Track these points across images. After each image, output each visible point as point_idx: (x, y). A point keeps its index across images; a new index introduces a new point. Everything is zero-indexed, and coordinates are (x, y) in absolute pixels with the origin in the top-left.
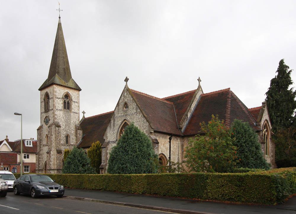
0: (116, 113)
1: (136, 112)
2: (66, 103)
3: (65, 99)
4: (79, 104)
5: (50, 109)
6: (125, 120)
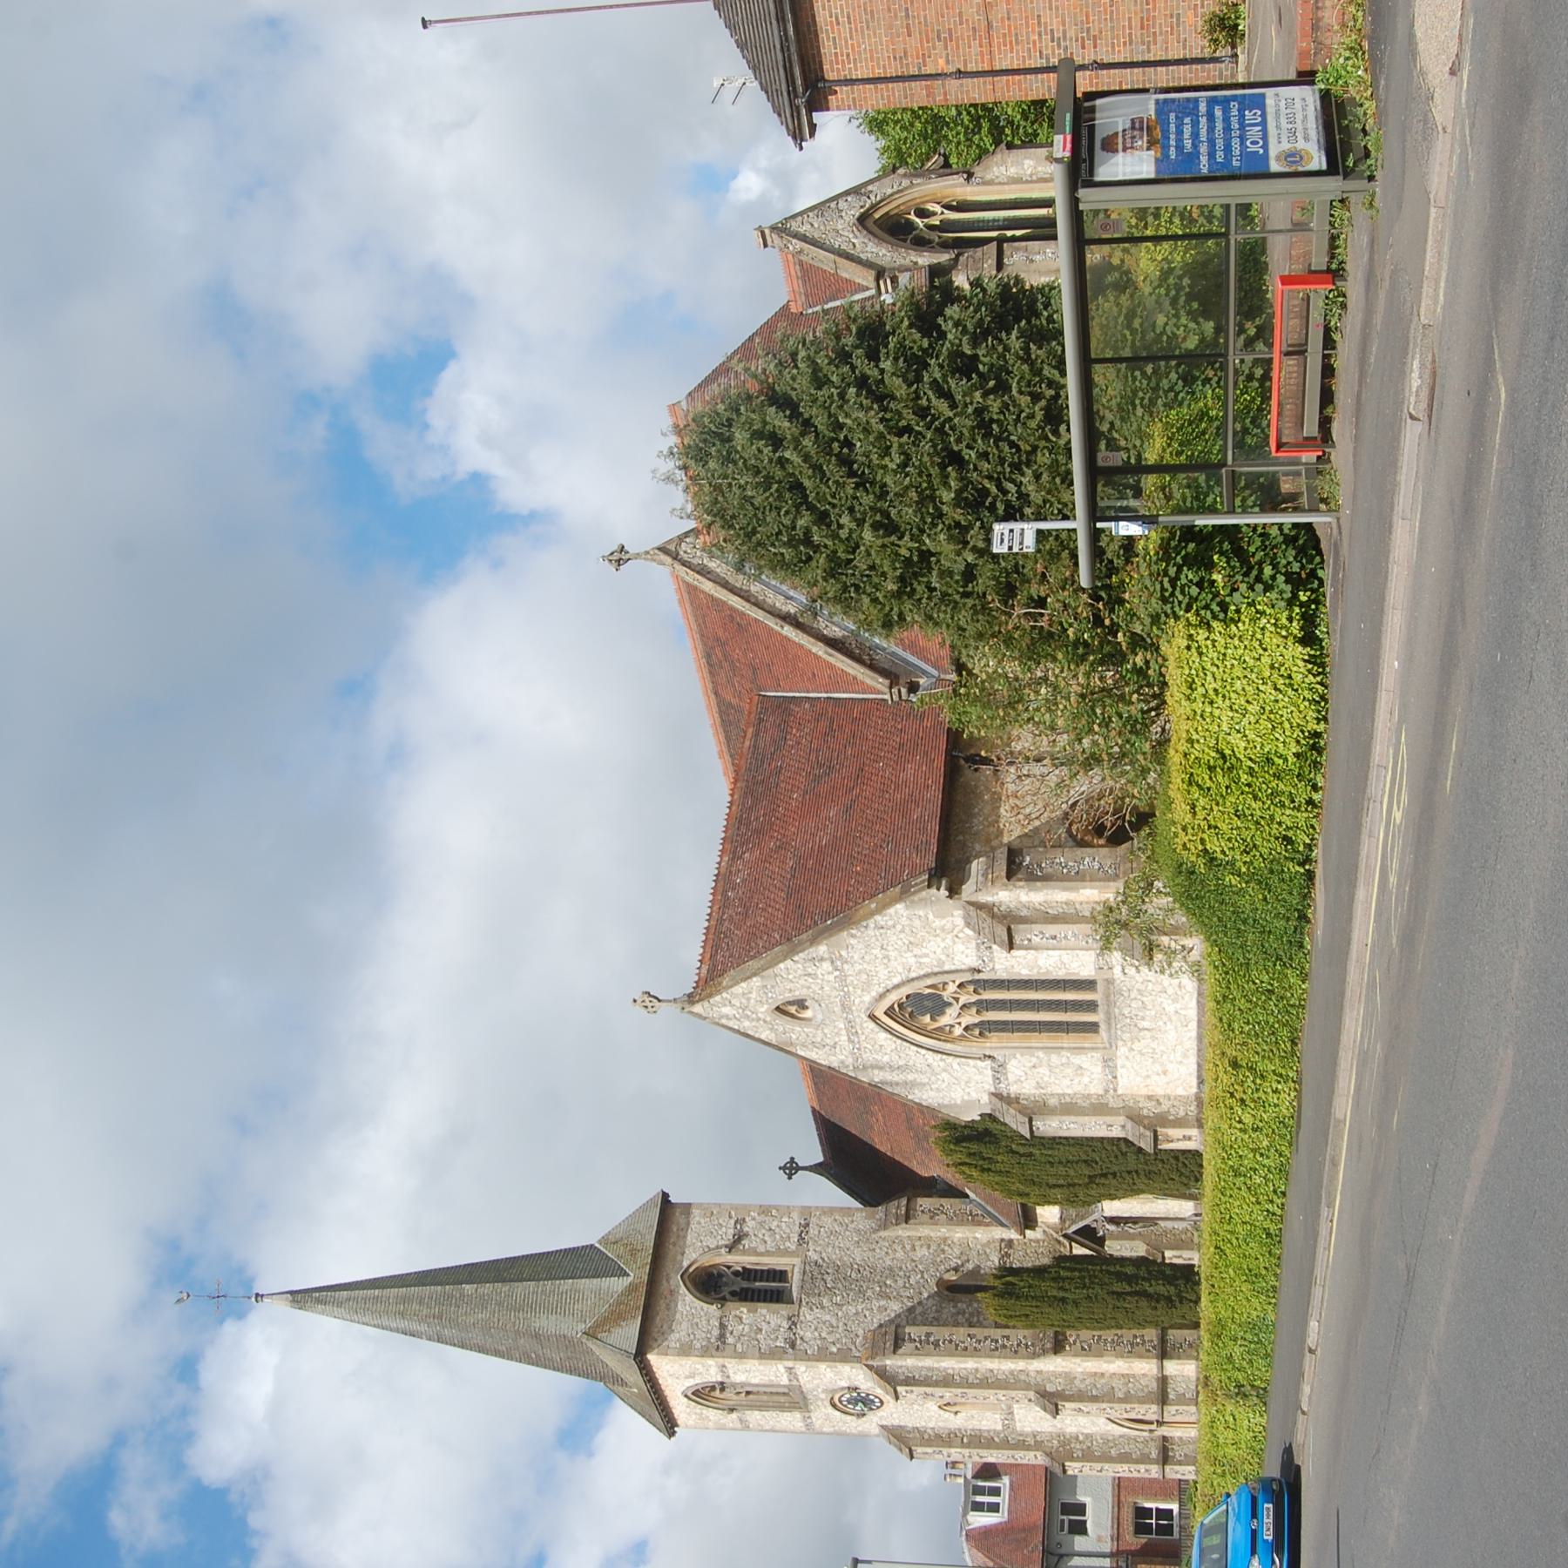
1: (832, 962)
2: (745, 1285)
3: (725, 1292)
4: (747, 1208)
5: (785, 1380)
6: (873, 1017)
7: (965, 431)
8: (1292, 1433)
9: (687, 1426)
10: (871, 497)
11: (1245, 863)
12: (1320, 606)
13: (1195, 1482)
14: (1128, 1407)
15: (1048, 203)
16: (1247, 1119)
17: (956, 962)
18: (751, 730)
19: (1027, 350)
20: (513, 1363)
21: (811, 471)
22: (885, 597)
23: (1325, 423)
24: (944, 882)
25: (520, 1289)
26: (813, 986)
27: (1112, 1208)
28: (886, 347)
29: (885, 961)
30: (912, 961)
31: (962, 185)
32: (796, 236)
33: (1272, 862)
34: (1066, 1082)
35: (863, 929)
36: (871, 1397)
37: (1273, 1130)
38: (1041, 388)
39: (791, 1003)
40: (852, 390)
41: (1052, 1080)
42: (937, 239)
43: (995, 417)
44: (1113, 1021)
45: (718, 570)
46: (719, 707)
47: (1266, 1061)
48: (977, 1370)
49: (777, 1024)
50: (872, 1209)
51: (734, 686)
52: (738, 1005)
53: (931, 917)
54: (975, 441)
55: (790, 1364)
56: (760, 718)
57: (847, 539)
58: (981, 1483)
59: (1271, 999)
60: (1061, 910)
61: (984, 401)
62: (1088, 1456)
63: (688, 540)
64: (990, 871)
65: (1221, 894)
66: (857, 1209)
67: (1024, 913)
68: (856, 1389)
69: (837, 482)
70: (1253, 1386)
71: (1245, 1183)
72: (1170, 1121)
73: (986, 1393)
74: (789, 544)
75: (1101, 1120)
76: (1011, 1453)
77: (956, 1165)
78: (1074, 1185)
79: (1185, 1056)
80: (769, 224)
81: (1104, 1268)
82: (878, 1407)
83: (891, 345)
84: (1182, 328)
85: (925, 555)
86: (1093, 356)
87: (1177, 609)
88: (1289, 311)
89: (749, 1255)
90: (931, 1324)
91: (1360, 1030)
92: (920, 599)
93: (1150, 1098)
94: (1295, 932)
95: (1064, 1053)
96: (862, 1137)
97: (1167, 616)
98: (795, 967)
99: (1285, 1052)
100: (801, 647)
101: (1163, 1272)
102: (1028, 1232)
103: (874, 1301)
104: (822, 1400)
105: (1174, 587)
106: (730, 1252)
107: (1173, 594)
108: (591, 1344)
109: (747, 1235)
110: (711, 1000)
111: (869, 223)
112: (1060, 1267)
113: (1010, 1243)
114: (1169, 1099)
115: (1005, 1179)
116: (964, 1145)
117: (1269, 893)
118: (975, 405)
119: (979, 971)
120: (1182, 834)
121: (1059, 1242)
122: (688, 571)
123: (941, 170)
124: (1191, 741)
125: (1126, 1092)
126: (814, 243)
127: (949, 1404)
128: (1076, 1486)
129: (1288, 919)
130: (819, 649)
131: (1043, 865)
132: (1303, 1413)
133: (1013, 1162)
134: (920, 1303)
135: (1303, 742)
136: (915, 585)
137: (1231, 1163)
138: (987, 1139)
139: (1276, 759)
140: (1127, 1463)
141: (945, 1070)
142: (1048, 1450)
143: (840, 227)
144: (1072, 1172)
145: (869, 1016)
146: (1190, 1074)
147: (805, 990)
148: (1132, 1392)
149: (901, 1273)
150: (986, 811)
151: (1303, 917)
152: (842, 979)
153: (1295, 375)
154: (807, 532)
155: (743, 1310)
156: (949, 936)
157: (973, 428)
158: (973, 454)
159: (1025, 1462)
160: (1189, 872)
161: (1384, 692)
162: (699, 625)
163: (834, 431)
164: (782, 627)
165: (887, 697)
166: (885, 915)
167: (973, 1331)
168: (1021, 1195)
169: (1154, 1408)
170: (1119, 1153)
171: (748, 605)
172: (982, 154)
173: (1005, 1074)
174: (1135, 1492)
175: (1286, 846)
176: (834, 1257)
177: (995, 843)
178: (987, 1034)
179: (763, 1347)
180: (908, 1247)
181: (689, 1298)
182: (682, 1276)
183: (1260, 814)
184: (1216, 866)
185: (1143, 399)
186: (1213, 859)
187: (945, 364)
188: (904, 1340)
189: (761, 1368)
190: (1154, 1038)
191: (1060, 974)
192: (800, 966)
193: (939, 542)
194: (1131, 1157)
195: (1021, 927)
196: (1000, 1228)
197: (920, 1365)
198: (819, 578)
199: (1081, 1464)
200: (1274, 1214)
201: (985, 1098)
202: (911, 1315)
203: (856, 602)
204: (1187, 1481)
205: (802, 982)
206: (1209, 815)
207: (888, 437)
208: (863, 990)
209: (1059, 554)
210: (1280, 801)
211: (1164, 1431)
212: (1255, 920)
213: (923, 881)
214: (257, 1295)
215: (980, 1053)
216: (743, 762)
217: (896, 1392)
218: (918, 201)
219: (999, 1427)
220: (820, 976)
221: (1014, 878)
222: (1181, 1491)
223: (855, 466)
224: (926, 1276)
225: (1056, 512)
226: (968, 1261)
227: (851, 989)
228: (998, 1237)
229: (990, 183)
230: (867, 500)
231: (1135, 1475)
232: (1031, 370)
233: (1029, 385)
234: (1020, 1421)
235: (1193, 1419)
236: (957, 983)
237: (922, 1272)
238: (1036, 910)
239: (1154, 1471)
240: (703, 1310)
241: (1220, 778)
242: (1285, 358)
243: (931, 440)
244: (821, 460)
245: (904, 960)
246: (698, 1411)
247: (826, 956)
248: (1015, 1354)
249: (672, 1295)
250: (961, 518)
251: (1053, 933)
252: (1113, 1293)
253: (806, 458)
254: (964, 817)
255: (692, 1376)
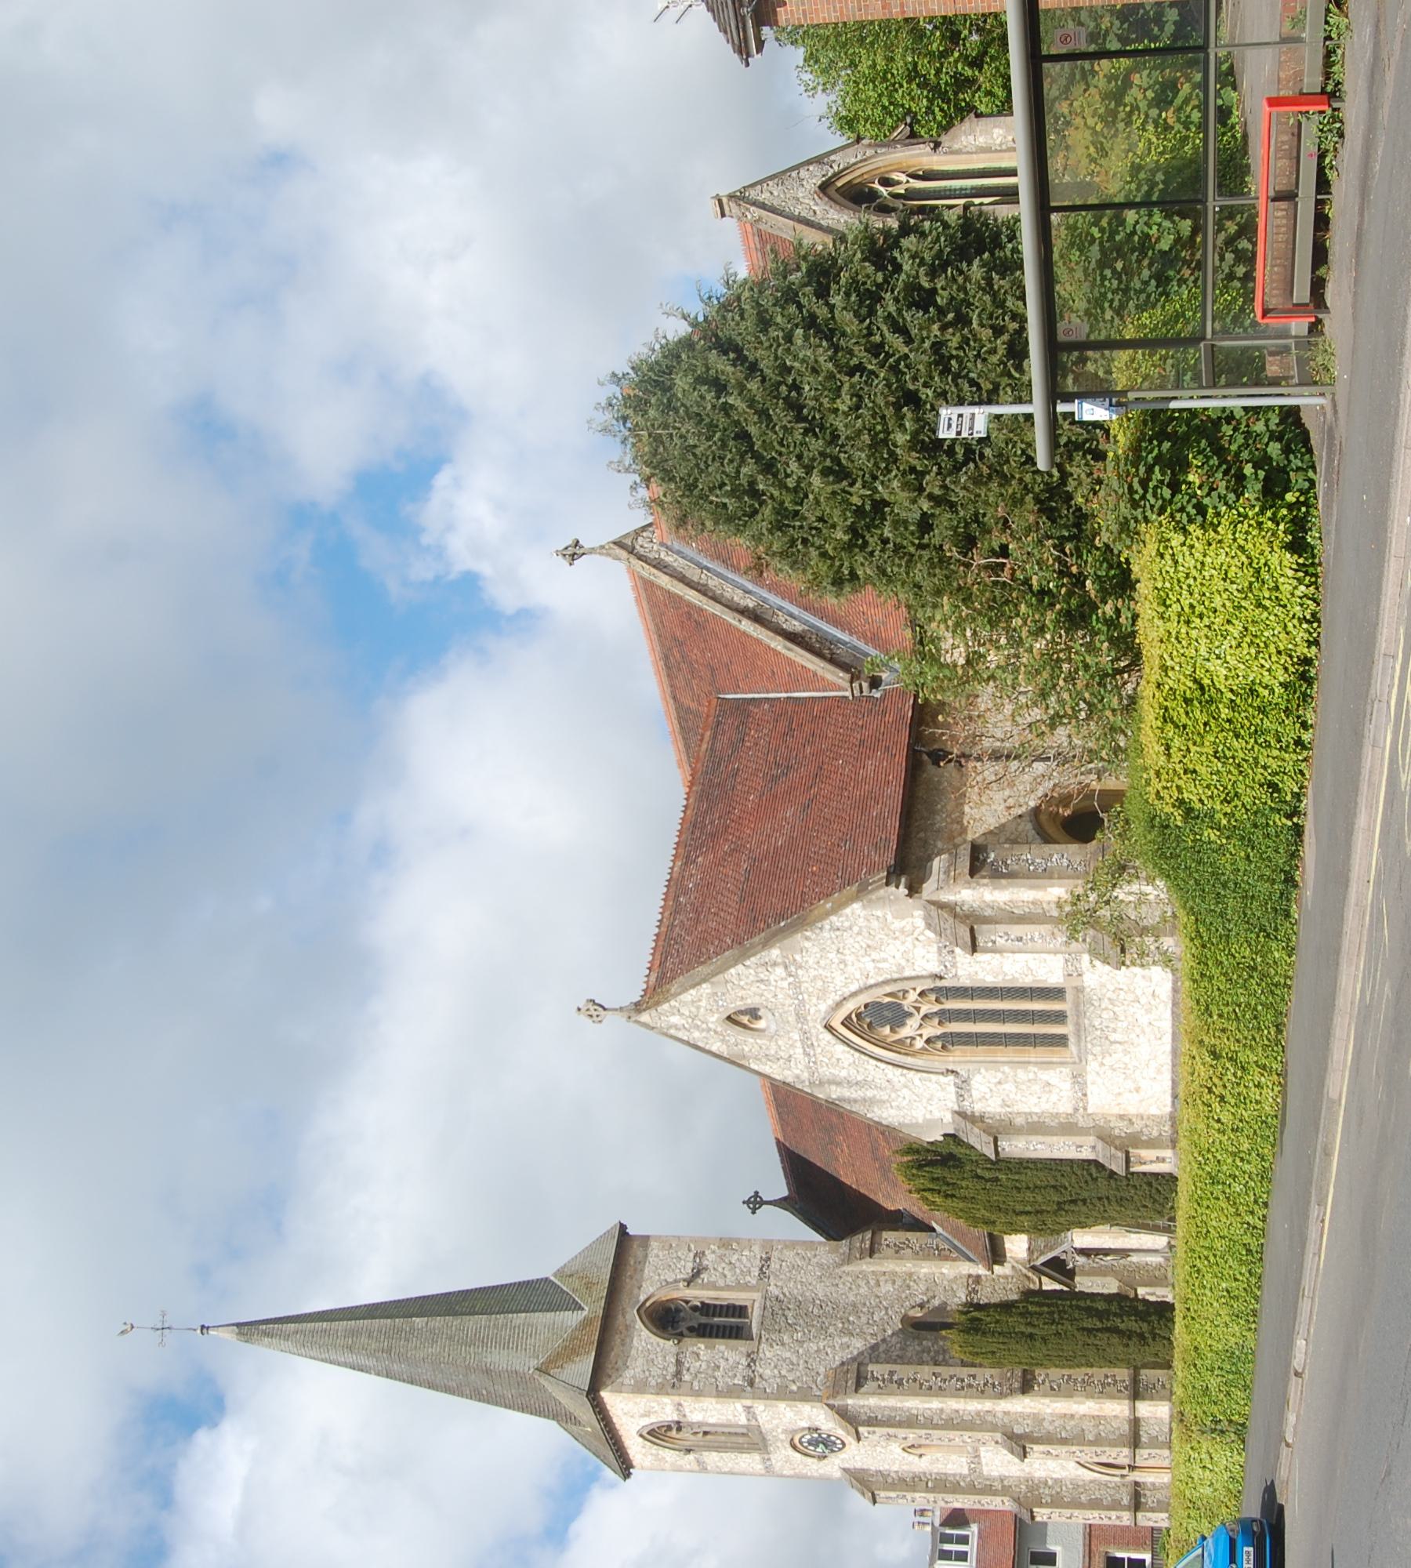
0: (787, 1072)
1: (786, 967)
2: (704, 1320)
3: (683, 1327)
4: (706, 1241)
5: (743, 1421)
6: (829, 1028)
7: (920, 367)
8: (1275, 1469)
9: (642, 1468)
10: (821, 442)
11: (1225, 814)
12: (1311, 510)
13: (1168, 1530)
14: (1099, 1450)
15: (1013, 173)
16: (1225, 1117)
17: (916, 967)
18: (708, 733)
19: (989, 281)
20: (464, 1400)
21: (756, 417)
22: (835, 549)
23: (1318, 286)
24: (903, 880)
25: (473, 1322)
26: (765, 993)
27: (1083, 1238)
28: (838, 283)
29: (842, 966)
30: (870, 966)
31: (928, 155)
32: (754, 203)
33: (1256, 813)
34: (1034, 1100)
35: (818, 931)
36: (833, 1438)
37: (1255, 1131)
38: (1004, 320)
39: (742, 1012)
40: (799, 332)
41: (1018, 1097)
42: (901, 207)
43: (954, 353)
44: (1082, 1033)
45: (675, 564)
46: (678, 713)
47: (1248, 1052)
48: (942, 1410)
49: (728, 1035)
50: (835, 1243)
51: (692, 689)
52: (687, 1013)
53: (889, 917)
54: (932, 378)
55: (748, 1403)
56: (718, 721)
57: (795, 488)
58: (949, 1531)
59: (1252, 977)
60: (1027, 910)
61: (942, 335)
62: (1057, 1502)
63: (644, 534)
64: (952, 868)
65: (1199, 852)
66: (820, 1243)
67: (988, 912)
68: (817, 1429)
69: (785, 428)
70: (1230, 1421)
71: (1224, 1192)
72: (1143, 1141)
73: (952, 1434)
74: (732, 494)
75: (1070, 1140)
76: (977, 1498)
77: (918, 1191)
78: (1041, 1212)
79: (1159, 1072)
80: (727, 193)
81: (1074, 1303)
82: (840, 1449)
83: (843, 281)
84: (1155, 228)
85: (880, 506)
86: (1044, 52)
87: (1148, 513)
88: (1277, 150)
89: (708, 1289)
90: (895, 1362)
91: (1359, 986)
92: (873, 552)
93: (1121, 1117)
94: (1281, 898)
95: (1032, 1068)
96: (826, 1169)
97: (1137, 521)
98: (746, 972)
99: (1269, 1040)
100: (759, 642)
101: (1135, 1308)
102: (996, 1267)
103: (837, 1339)
104: (782, 1441)
105: (1145, 489)
106: (688, 1285)
107: (1143, 497)
108: (543, 1381)
109: (706, 1269)
110: (659, 1009)
111: (831, 191)
112: (1028, 1302)
113: (978, 1279)
114: (1142, 1119)
115: (970, 1205)
116: (927, 1169)
117: (1253, 848)
118: (932, 339)
119: (941, 978)
120: (1154, 781)
121: (1028, 1278)
122: (644, 565)
123: (908, 141)
124: (1165, 669)
125: (1097, 1111)
126: (773, 210)
127: (913, 1446)
128: (1046, 1535)
129: (1273, 882)
130: (778, 644)
131: (1009, 862)
132: (1288, 1445)
133: (978, 1187)
134: (884, 1340)
135: (1291, 669)
136: (868, 536)
137: (1208, 1169)
138: (951, 1163)
139: (1261, 690)
140: (1099, 1509)
141: (906, 1087)
142: (1016, 1496)
143: (801, 195)
144: (1039, 1198)
145: (825, 1027)
146: (1164, 1092)
147: (757, 998)
148: (1103, 1434)
149: (865, 1310)
150: (949, 808)
151: (1290, 880)
152: (797, 986)
153: (1283, 229)
154: (752, 483)
155: (700, 1346)
156: (909, 939)
157: (930, 364)
158: (930, 392)
159: (991, 1507)
160: (1162, 826)
161: (1393, 559)
162: (656, 625)
163: (781, 374)
164: (740, 621)
165: (848, 694)
166: (841, 916)
167: (938, 1369)
168: (987, 1222)
169: (1126, 1451)
170: (1089, 1178)
171: (704, 599)
172: (946, 128)
173: (969, 1091)
174: (1108, 1543)
175: (1271, 794)
176: (796, 1292)
177: (958, 840)
178: (950, 1047)
179: (720, 1385)
180: (872, 1283)
181: (645, 1333)
182: (638, 1311)
183: (1243, 756)
184: (1192, 818)
185: (1112, 301)
186: (1190, 810)
187: (901, 298)
188: (866, 1379)
189: (719, 1406)
190: (1126, 1052)
191: (1027, 981)
192: (752, 971)
193: (892, 489)
194: (1102, 1183)
195: (985, 927)
196: (968, 1263)
197: (883, 1404)
198: (764, 531)
199: (1050, 1510)
200: (1255, 1227)
201: (948, 1118)
202: (875, 1353)
203: (804, 555)
204: (1159, 1530)
205: (754, 989)
206: (1185, 757)
207: (838, 376)
208: (818, 998)
209: (1022, 499)
210: (1266, 741)
211: (1136, 1476)
212: (1236, 884)
213: (882, 879)
214: (203, 1327)
215: (943, 1067)
216: (699, 765)
217: (857, 1432)
218: (883, 170)
219: (965, 1471)
220: (774, 983)
221: (978, 876)
222: (1154, 1541)
223: (805, 411)
224: (890, 1313)
225: (1019, 452)
226: (934, 1297)
227: (806, 996)
228: (965, 1272)
229: (958, 152)
230: (816, 445)
231: (1106, 1522)
232: (994, 302)
233: (991, 317)
234: (987, 1464)
235: (1166, 1463)
236: (918, 991)
237: (886, 1309)
238: (1002, 910)
239: (1126, 1518)
240: (658, 1344)
241: (1197, 713)
242: (1271, 204)
243: (884, 379)
244: (768, 405)
245: (862, 965)
246: (654, 1452)
247: (779, 960)
248: (982, 1394)
249: (627, 1330)
250: (915, 462)
251: (1019, 935)
252: (1084, 1329)
253: (752, 403)
254: (926, 814)
255: (647, 1414)
